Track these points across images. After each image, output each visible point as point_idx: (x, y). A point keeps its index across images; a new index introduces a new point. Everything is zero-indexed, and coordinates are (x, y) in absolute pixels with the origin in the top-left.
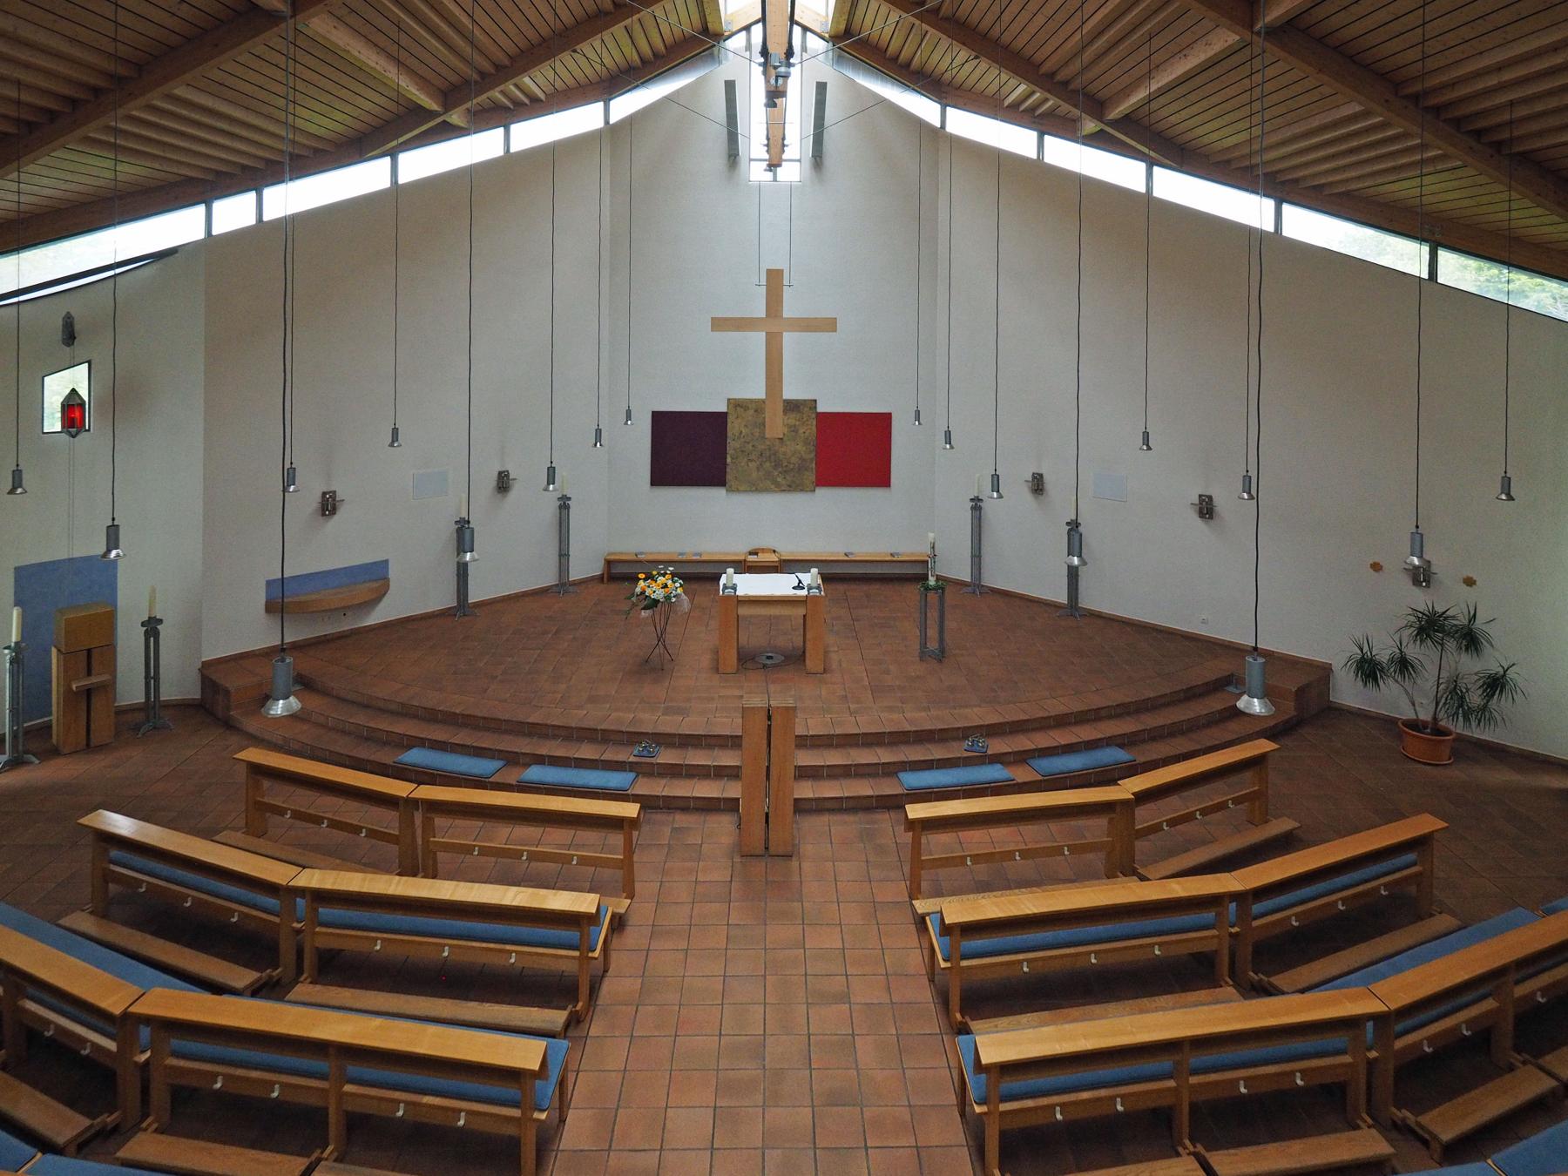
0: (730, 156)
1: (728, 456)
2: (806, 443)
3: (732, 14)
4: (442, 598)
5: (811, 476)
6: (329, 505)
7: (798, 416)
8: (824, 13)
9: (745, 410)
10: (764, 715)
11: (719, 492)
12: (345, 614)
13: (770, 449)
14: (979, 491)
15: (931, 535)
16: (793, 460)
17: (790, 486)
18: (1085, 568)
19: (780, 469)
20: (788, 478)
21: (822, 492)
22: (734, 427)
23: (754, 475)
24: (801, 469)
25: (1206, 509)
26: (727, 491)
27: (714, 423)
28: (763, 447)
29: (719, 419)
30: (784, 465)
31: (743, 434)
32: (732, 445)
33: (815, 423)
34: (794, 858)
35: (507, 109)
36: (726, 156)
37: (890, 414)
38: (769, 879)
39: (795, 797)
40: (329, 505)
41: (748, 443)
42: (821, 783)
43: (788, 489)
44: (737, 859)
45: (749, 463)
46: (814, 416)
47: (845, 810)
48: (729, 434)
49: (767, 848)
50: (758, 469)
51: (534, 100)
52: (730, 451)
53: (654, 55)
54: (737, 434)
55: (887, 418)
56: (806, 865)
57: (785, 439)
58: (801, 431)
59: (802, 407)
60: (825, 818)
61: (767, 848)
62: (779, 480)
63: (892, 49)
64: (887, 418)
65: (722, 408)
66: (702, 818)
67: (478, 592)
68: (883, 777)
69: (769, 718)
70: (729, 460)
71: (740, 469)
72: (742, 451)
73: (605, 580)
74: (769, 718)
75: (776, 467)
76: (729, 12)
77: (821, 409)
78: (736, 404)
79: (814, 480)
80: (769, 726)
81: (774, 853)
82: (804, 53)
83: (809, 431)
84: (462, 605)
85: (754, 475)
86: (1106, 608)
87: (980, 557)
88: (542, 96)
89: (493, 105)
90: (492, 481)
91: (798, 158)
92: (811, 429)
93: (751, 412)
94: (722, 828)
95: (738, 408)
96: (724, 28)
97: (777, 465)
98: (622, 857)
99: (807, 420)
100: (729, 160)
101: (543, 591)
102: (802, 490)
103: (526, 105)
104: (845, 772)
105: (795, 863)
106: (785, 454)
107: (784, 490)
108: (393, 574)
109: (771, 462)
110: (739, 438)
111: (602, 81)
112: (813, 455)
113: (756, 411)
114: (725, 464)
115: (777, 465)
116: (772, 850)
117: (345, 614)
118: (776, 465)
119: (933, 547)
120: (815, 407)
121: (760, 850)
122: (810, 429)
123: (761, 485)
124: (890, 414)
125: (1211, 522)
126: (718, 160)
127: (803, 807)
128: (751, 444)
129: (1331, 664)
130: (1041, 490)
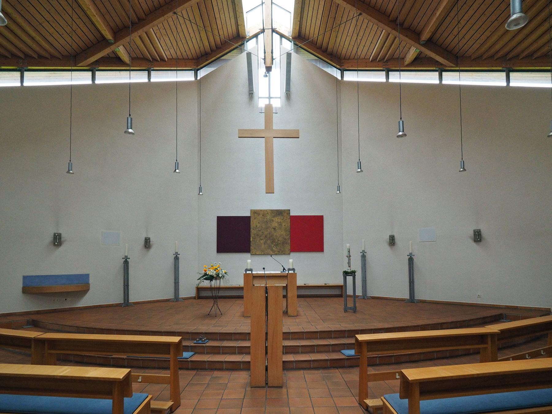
0: (250, 94)
1: (251, 238)
2: (285, 230)
3: (249, 28)
4: (116, 298)
5: (288, 247)
6: (57, 240)
7: (282, 218)
8: (290, 28)
9: (258, 215)
10: (263, 291)
11: (247, 255)
12: (66, 300)
13: (270, 234)
14: (364, 248)
15: (348, 245)
16: (280, 239)
17: (279, 252)
18: (461, 161)
19: (274, 244)
20: (278, 247)
21: (292, 254)
22: (254, 223)
23: (263, 246)
24: (284, 243)
25: (478, 237)
26: (251, 254)
27: (244, 221)
28: (266, 233)
29: (247, 219)
30: (276, 241)
31: (258, 226)
32: (253, 232)
33: (289, 221)
34: (283, 388)
35: (149, 61)
36: (248, 94)
37: (322, 216)
38: (267, 397)
39: (283, 360)
40: (57, 240)
41: (260, 231)
42: (298, 355)
43: (278, 253)
44: (249, 389)
45: (261, 241)
46: (289, 217)
47: (312, 368)
48: (252, 227)
49: (267, 384)
50: (265, 244)
51: (162, 60)
52: (252, 235)
53: (216, 47)
54: (255, 227)
55: (320, 219)
56: (291, 391)
57: (277, 228)
58: (284, 225)
59: (283, 213)
60: (302, 372)
61: (267, 384)
62: (274, 249)
63: (319, 42)
64: (320, 219)
65: (248, 214)
66: (230, 373)
67: (420, 295)
68: (332, 352)
69: (267, 293)
70: (251, 239)
71: (257, 243)
72: (257, 235)
73: (196, 299)
74: (267, 293)
75: (272, 243)
76: (248, 28)
77: (292, 214)
78: (255, 212)
79: (290, 249)
80: (267, 298)
81: (270, 386)
82: (281, 45)
83: (286, 225)
84: (126, 303)
85: (263, 246)
86: (428, 298)
87: (366, 281)
88: (166, 59)
89: (142, 56)
90: (49, 238)
91: (280, 96)
92: (288, 224)
93: (261, 215)
94: (242, 377)
95: (255, 214)
96: (246, 34)
97: (273, 241)
98: (170, 376)
99: (286, 220)
100: (249, 95)
101: (167, 300)
102: (284, 254)
103: (158, 61)
104: (312, 349)
105: (284, 390)
106: (276, 236)
107: (276, 254)
108: (91, 281)
109: (270, 240)
110: (256, 228)
111: (193, 59)
112: (288, 237)
113: (263, 215)
114: (250, 242)
115: (273, 241)
116: (270, 384)
117: (66, 300)
118: (272, 242)
119: (349, 251)
120: (289, 213)
121: (264, 385)
122: (287, 224)
123: (266, 251)
124: (322, 216)
125: (481, 243)
126: (246, 97)
127: (287, 366)
128: (261, 232)
129: (550, 309)
130: (394, 244)
